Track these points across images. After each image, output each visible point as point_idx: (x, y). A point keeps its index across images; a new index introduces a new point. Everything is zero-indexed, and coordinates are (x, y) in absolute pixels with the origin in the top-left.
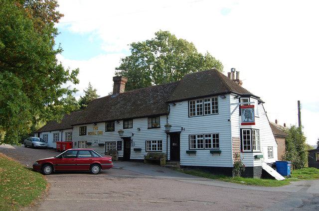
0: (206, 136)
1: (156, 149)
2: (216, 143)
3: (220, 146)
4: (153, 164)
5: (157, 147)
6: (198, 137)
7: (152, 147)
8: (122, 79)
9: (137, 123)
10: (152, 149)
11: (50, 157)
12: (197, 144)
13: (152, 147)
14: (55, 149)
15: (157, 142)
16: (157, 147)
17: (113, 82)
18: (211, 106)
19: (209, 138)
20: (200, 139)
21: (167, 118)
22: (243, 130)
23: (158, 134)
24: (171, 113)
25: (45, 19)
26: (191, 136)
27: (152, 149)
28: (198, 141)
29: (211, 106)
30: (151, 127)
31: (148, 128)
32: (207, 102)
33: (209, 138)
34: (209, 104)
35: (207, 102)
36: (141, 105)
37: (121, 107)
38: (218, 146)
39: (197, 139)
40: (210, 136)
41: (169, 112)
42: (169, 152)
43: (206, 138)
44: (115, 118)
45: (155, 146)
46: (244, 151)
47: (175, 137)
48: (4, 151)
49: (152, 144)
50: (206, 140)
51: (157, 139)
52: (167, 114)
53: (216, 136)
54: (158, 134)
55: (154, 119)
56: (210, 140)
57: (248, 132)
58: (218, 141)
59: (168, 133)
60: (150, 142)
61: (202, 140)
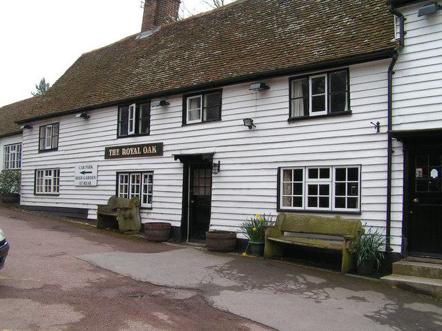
1: (325, 203)
4: (316, 248)
5: (332, 196)
6: (313, 173)
7: (305, 195)
9: (236, 104)
10: (305, 202)
11: (142, 126)
13: (305, 195)
15: (333, 173)
16: (332, 196)
19: (324, 181)
21: (391, 73)
26: (288, 172)
27: (305, 202)
28: (312, 189)
30: (299, 113)
33: (324, 181)
36: (246, 42)
37: (171, 58)
38: (353, 203)
39: (307, 181)
40: (325, 173)
41: (401, 43)
42: (398, 216)
44: (156, 88)
45: (325, 189)
48: (440, 321)
52: (388, 55)
55: (323, 89)
58: (354, 190)
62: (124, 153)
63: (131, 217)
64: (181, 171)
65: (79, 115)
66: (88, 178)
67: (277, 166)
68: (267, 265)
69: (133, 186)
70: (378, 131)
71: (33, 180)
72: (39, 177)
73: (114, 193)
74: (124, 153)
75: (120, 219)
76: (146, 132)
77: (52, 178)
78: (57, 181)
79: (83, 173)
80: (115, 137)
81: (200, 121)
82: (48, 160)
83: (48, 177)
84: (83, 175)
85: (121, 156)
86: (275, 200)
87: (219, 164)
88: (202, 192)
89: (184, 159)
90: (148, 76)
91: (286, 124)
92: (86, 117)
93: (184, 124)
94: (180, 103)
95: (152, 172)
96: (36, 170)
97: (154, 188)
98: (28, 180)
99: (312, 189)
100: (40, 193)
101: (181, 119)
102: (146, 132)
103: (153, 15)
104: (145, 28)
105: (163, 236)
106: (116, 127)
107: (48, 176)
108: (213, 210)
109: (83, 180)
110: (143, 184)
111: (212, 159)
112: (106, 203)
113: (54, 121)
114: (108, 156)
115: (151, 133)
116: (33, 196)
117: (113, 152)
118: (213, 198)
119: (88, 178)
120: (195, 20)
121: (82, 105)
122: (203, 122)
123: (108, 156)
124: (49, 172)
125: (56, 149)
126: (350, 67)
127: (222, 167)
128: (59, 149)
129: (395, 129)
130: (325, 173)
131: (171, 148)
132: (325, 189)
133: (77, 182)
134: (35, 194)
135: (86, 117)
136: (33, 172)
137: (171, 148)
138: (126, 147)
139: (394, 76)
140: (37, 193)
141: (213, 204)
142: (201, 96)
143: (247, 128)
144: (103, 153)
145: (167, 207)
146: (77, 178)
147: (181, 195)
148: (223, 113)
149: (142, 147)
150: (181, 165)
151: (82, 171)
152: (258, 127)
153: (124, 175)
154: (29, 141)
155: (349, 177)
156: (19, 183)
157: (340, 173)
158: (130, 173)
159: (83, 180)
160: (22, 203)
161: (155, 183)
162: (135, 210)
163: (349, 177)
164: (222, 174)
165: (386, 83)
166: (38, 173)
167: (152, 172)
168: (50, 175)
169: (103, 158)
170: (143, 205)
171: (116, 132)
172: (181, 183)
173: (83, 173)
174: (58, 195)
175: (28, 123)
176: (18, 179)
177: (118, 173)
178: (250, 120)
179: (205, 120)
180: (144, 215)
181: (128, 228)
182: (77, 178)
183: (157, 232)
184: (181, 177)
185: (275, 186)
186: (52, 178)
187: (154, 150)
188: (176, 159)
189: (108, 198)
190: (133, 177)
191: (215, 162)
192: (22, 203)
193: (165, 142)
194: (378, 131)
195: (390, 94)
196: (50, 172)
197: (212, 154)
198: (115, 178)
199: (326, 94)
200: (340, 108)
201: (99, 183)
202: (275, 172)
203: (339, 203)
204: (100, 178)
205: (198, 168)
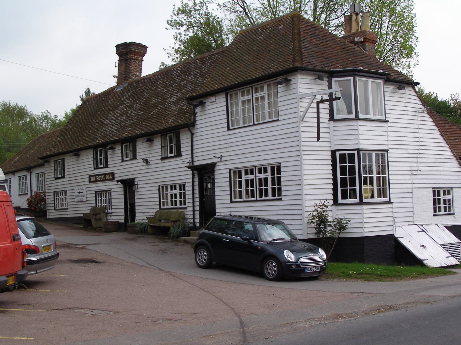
2: (250, 188)
3: (283, 194)
8: (23, 203)
9: (142, 149)
10: (178, 203)
12: (244, 189)
14: (24, 210)
17: (117, 58)
20: (250, 177)
21: (192, 134)
22: (338, 153)
23: (177, 171)
24: (198, 122)
25: (15, 113)
27: (178, 203)
28: (247, 181)
31: (163, 159)
34: (263, 98)
37: (122, 115)
41: (195, 121)
43: (259, 176)
46: (340, 201)
47: (204, 173)
49: (244, 177)
50: (260, 180)
51: (177, 181)
53: (276, 169)
54: (177, 171)
56: (176, 195)
57: (351, 157)
59: (193, 168)
60: (240, 172)
61: (252, 180)
62: (98, 179)
63: (100, 219)
64: (122, 189)
65: (73, 154)
66: (82, 196)
67: (158, 184)
68: (175, 245)
70: (221, 160)
71: (53, 199)
72: (163, 191)
73: (94, 205)
74: (98, 179)
75: (93, 222)
76: (107, 166)
77: (177, 192)
79: (79, 193)
80: (93, 169)
81: (252, 124)
82: (61, 185)
83: (174, 192)
84: (78, 194)
85: (96, 181)
86: (158, 203)
87: (137, 185)
89: (123, 182)
90: (111, 127)
91: (160, 161)
92: (77, 155)
93: (123, 161)
94: (120, 148)
95: (111, 190)
96: (54, 192)
97: (112, 201)
98: (50, 199)
100: (58, 208)
101: (121, 158)
102: (107, 166)
103: (123, 73)
104: (119, 83)
105: (118, 227)
106: (92, 162)
107: (173, 191)
108: (136, 211)
109: (79, 198)
111: (134, 182)
112: (88, 212)
113: (62, 157)
114: (90, 182)
115: (109, 166)
116: (54, 211)
117: (93, 179)
118: (136, 204)
119: (82, 196)
120: (155, 75)
121: (75, 147)
122: (131, 160)
123: (90, 182)
124: (173, 187)
125: (63, 177)
126: (180, 130)
128: (66, 177)
129: (195, 164)
131: (118, 177)
133: (76, 200)
134: (55, 209)
135: (77, 155)
136: (53, 194)
137: (118, 177)
138: (98, 175)
139: (194, 136)
140: (56, 208)
141: (136, 208)
142: (128, 144)
143: (145, 164)
144: (88, 179)
145: (117, 214)
146: (76, 196)
147: (123, 204)
148: (137, 154)
149: (105, 174)
150: (121, 186)
151: (78, 191)
152: (151, 162)
154: (49, 171)
156: (45, 202)
159: (79, 198)
160: (48, 217)
161: (112, 197)
162: (102, 215)
164: (139, 190)
165: (190, 140)
166: (55, 193)
167: (111, 190)
168: (175, 189)
169: (87, 183)
170: (109, 211)
171: (93, 166)
172: (123, 196)
173: (79, 193)
174: (67, 209)
175: (45, 160)
176: (44, 200)
177: (96, 192)
179: (132, 158)
180: (109, 218)
181: (98, 226)
182: (76, 196)
183: (109, 226)
184: (123, 193)
185: (157, 195)
187: (111, 177)
188: (117, 183)
189: (90, 208)
191: (136, 183)
192: (48, 217)
193: (115, 172)
194: (221, 160)
195: (192, 146)
197: (134, 179)
198: (94, 195)
199: (173, 144)
201: (88, 199)
202: (157, 188)
204: (88, 196)
205: (129, 185)
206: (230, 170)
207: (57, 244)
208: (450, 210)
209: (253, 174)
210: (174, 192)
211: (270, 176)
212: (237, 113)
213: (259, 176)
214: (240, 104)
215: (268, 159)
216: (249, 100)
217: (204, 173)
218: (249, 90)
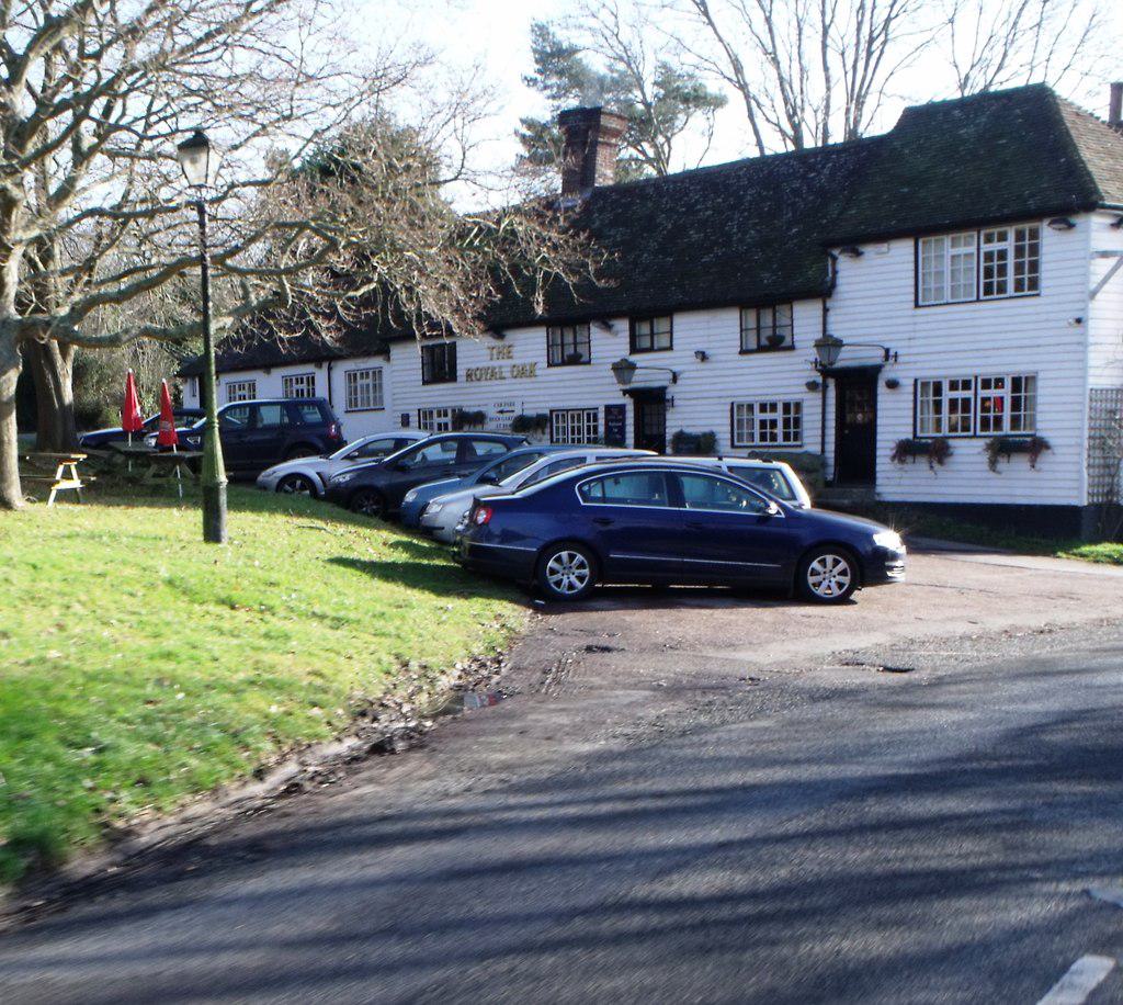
0: (986, 384)
6: (954, 386)
10: (757, 437)
16: (779, 430)
18: (1011, 261)
21: (826, 310)
23: (785, 377)
28: (953, 403)
29: (1011, 261)
32: (995, 246)
35: (995, 246)
38: (797, 436)
43: (983, 393)
47: (855, 388)
49: (947, 395)
52: (823, 291)
54: (785, 377)
67: (730, 400)
69: (589, 427)
72: (558, 433)
78: (378, 387)
79: (501, 412)
88: (655, 431)
99: (763, 424)
110: (979, 414)
120: (675, 175)
127: (676, 403)
130: (999, 383)
132: (774, 423)
153: (576, 413)
155: (793, 410)
157: (787, 407)
158: (568, 411)
163: (793, 410)
168: (362, 386)
173: (501, 412)
178: (703, 353)
186: (370, 381)
190: (588, 415)
191: (668, 397)
196: (367, 374)
200: (776, 344)
203: (786, 437)
206: (916, 381)
207: (195, 517)
208: (796, 439)
209: (970, 389)
210: (300, 386)
211: (1010, 394)
212: (939, 274)
213: (983, 393)
214: (947, 261)
215: (1022, 367)
216: (969, 255)
217: (855, 388)
218: (972, 237)
